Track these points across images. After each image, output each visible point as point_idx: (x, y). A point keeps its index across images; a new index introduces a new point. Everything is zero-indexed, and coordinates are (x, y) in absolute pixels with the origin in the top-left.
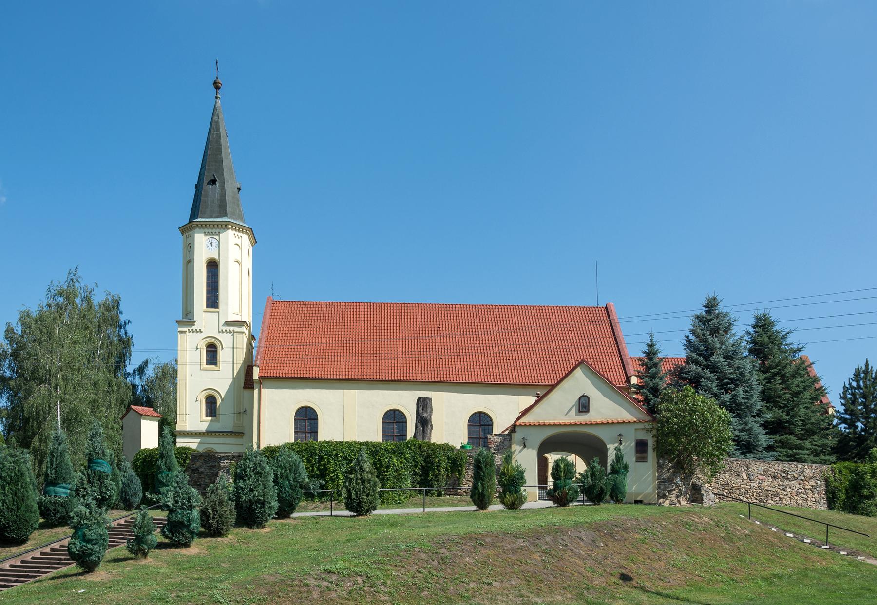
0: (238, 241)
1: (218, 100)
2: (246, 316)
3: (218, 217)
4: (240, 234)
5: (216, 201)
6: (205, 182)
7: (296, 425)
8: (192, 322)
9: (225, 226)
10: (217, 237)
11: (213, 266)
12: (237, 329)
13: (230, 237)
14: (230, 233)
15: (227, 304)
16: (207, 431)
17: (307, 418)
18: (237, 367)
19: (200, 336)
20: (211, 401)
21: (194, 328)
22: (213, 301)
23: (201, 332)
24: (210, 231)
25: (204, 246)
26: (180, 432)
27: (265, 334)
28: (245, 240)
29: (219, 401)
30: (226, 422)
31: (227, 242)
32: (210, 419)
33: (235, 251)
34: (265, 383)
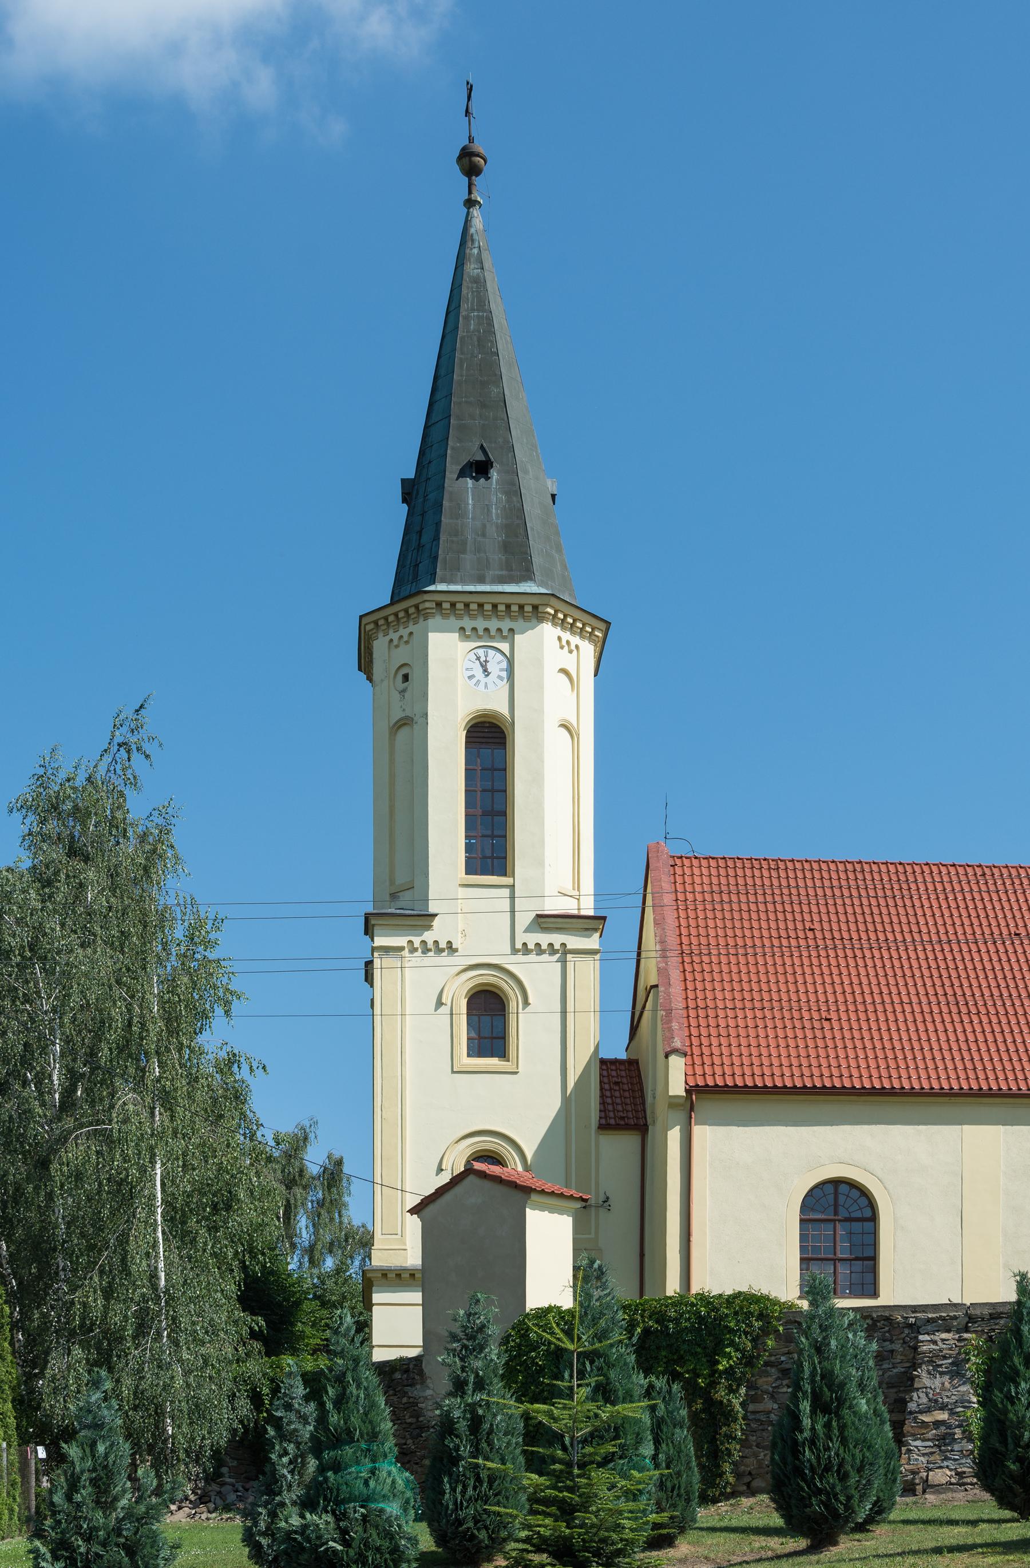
0: (568, 661)
1: (475, 212)
3: (502, 580)
4: (575, 640)
5: (492, 531)
9: (532, 611)
10: (505, 647)
12: (574, 942)
14: (548, 632)
15: (540, 863)
17: (841, 1220)
18: (579, 1061)
21: (429, 936)
22: (490, 848)
24: (481, 624)
25: (461, 676)
27: (674, 961)
31: (538, 663)
33: (551, 684)
34: (704, 1106)
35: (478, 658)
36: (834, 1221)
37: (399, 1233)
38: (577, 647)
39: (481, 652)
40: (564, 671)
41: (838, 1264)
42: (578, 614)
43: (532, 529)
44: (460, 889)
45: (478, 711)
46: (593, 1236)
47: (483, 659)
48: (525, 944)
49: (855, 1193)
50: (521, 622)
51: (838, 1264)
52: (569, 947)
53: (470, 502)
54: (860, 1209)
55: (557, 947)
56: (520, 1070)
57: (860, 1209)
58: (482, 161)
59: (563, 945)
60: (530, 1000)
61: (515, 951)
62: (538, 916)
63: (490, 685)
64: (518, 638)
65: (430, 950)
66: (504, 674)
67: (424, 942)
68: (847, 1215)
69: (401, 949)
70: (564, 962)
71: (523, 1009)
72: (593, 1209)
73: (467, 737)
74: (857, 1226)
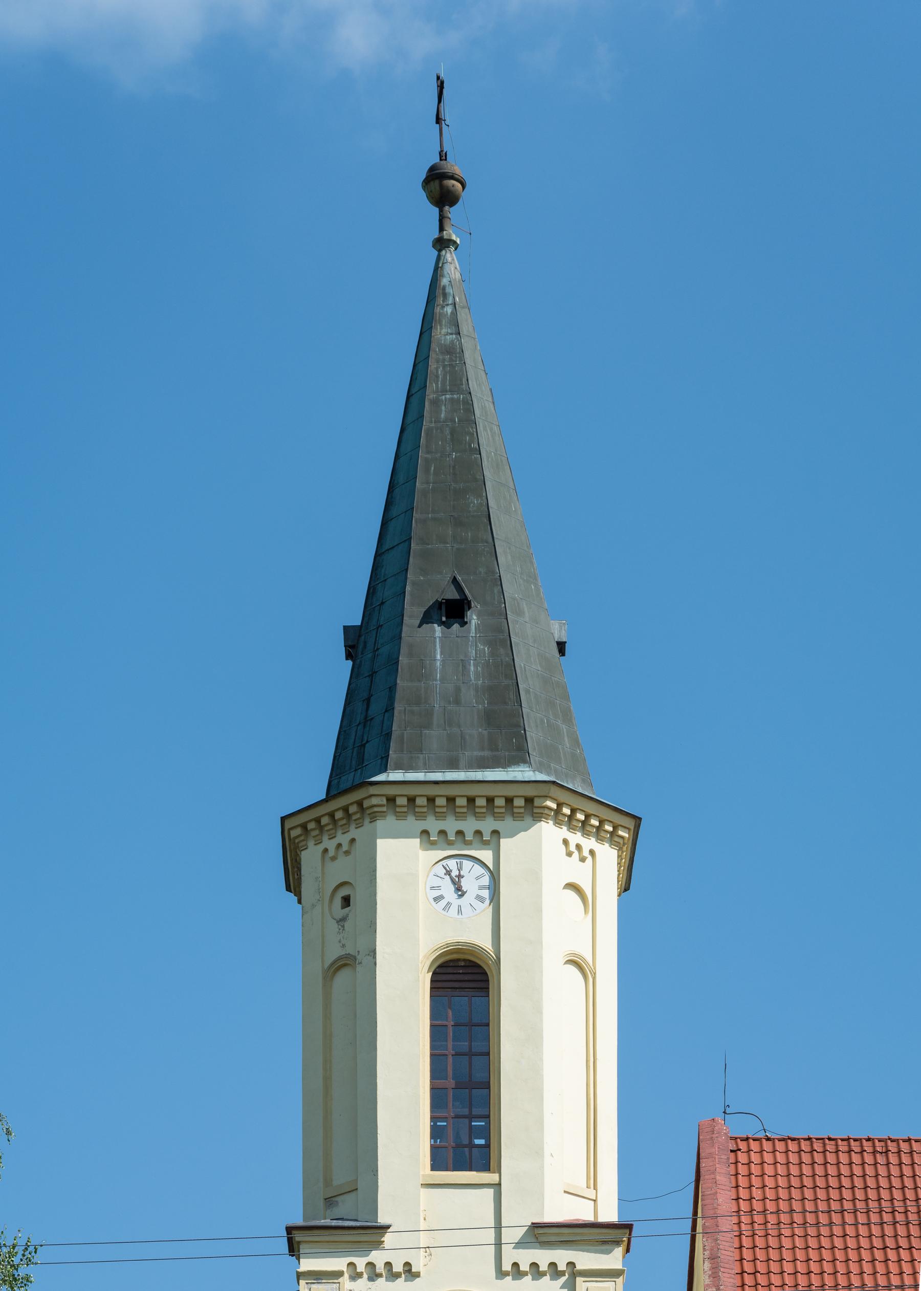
0: (581, 874)
1: (449, 255)
3: (483, 764)
4: (589, 843)
5: (468, 695)
6: (413, 612)
8: (372, 1233)
9: (526, 806)
10: (486, 856)
11: (464, 983)
12: (586, 1260)
14: (549, 834)
15: (538, 1152)
21: (378, 1257)
22: (466, 1134)
24: (451, 825)
25: (424, 896)
31: (534, 877)
35: (448, 873)
38: (592, 852)
39: (452, 864)
40: (573, 887)
42: (591, 808)
43: (527, 692)
44: (424, 1192)
45: (448, 945)
47: (455, 873)
52: (579, 1267)
53: (438, 657)
55: (562, 1267)
59: (571, 1264)
62: (535, 1226)
65: (379, 1275)
66: (486, 894)
67: (371, 1265)
69: (338, 1274)
73: (432, 981)
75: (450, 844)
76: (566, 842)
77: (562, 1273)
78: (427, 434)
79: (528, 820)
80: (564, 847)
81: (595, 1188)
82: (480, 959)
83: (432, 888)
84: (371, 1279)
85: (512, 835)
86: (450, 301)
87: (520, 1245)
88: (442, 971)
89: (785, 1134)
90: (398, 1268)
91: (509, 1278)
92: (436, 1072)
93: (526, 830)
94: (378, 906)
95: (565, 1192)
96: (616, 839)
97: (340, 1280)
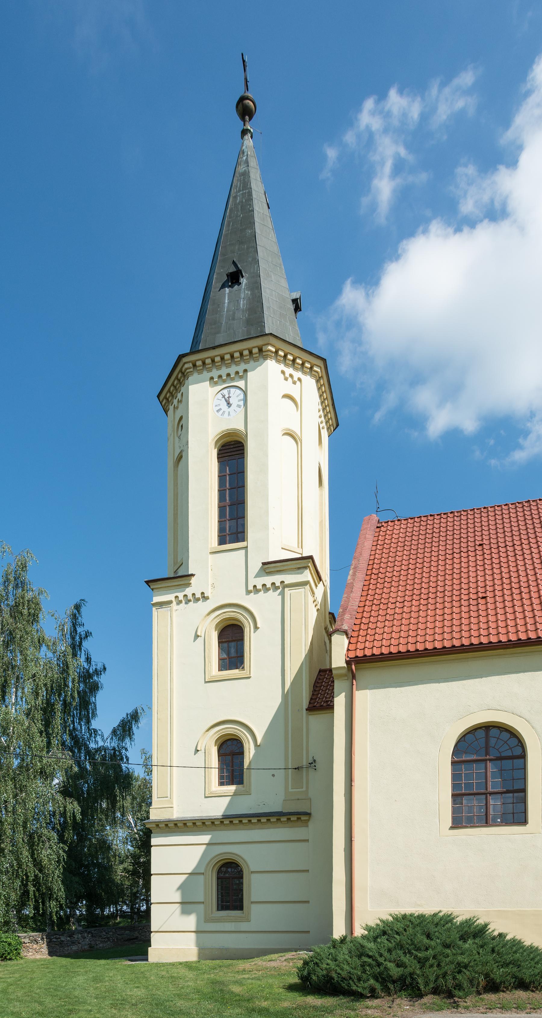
0: (294, 391)
2: (316, 544)
4: (297, 374)
5: (239, 315)
7: (455, 777)
8: (180, 577)
9: (262, 354)
10: (241, 384)
11: (232, 451)
12: (289, 578)
13: (271, 377)
14: (272, 367)
15: (266, 527)
16: (225, 817)
19: (204, 607)
20: (230, 751)
21: (189, 591)
22: (233, 525)
23: (204, 597)
24: (224, 371)
26: (157, 824)
28: (308, 388)
29: (250, 752)
30: (267, 790)
32: (233, 788)
34: (365, 675)
35: (224, 396)
36: (486, 760)
37: (169, 796)
38: (299, 379)
39: (225, 392)
40: (287, 396)
41: (490, 798)
42: (297, 352)
43: (269, 308)
44: (210, 556)
45: (223, 432)
46: (304, 789)
47: (227, 396)
48: (255, 586)
49: (505, 735)
50: (252, 362)
51: (490, 798)
52: (286, 583)
53: (226, 301)
54: (511, 748)
55: (278, 584)
56: (251, 675)
57: (511, 748)
58: (251, 104)
59: (282, 582)
60: (259, 625)
61: (248, 592)
62: (264, 564)
63: (232, 413)
64: (249, 374)
65: (190, 601)
66: (242, 403)
67: (185, 596)
68: (499, 755)
69: (170, 602)
70: (282, 594)
71: (254, 632)
72: (305, 769)
73: (218, 454)
74: (508, 764)
75: (224, 381)
76: (283, 372)
77: (277, 588)
78: (230, 211)
79: (261, 360)
80: (282, 375)
81: (302, 548)
82: (321, 522)
83: (216, 406)
84: (186, 603)
85: (253, 370)
86: (246, 154)
87: (256, 576)
88: (224, 448)
89: (408, 516)
90: (198, 595)
91: (252, 594)
92: (221, 497)
93: (260, 366)
94: (189, 419)
95: (282, 548)
96: (313, 373)
97: (171, 605)
